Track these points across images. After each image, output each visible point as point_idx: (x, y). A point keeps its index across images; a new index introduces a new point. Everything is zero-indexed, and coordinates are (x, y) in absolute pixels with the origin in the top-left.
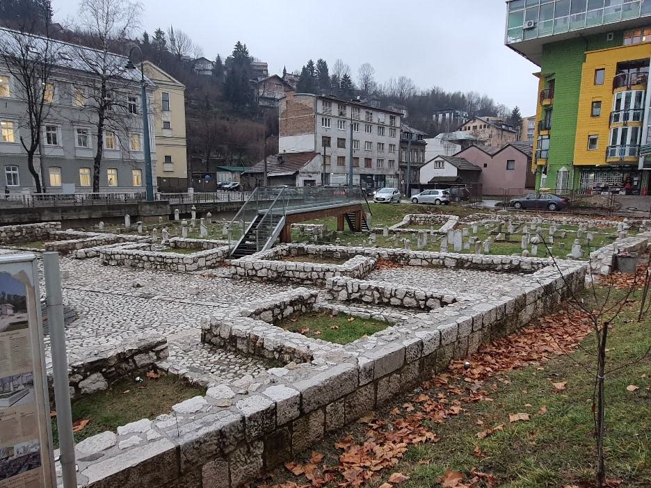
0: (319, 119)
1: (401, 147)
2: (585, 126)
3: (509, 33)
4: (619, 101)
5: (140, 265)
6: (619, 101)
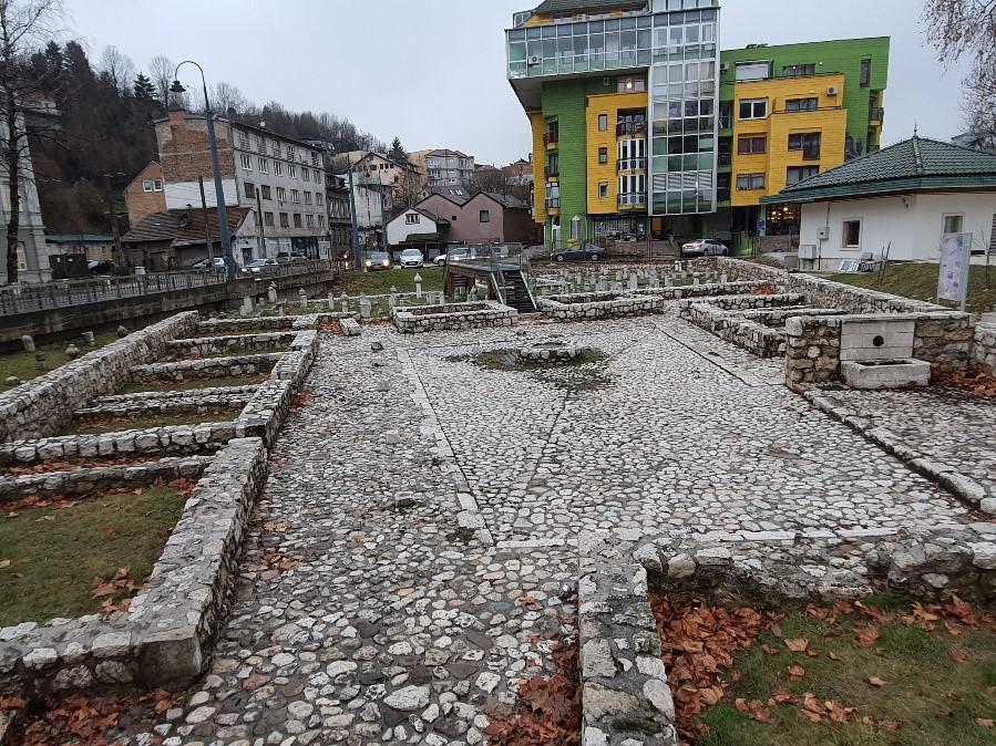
0: (237, 155)
1: (328, 197)
2: (597, 174)
3: (512, 66)
4: (625, 149)
5: (456, 327)
6: (625, 149)
